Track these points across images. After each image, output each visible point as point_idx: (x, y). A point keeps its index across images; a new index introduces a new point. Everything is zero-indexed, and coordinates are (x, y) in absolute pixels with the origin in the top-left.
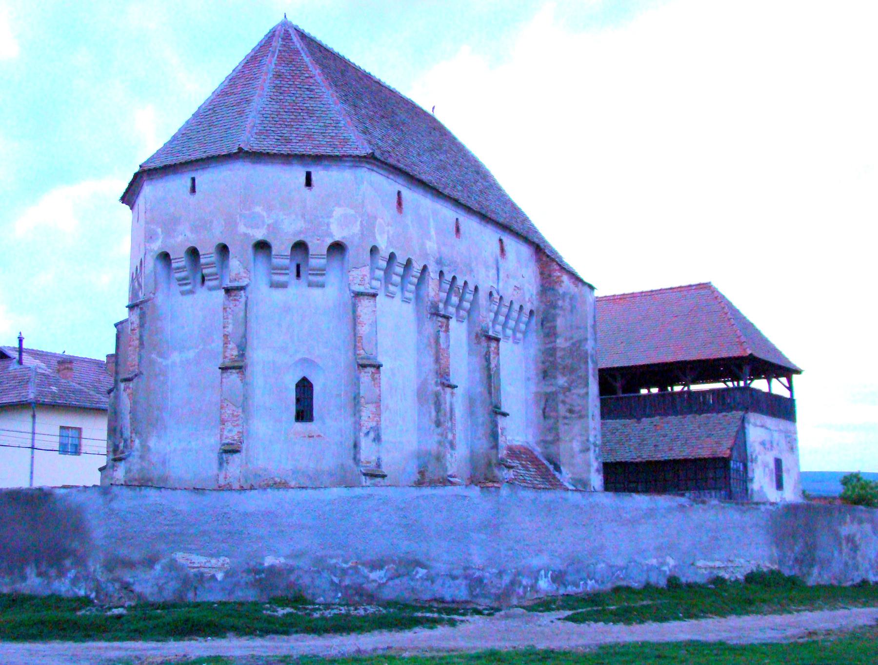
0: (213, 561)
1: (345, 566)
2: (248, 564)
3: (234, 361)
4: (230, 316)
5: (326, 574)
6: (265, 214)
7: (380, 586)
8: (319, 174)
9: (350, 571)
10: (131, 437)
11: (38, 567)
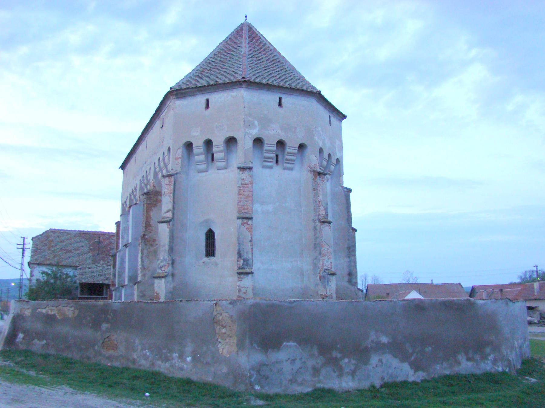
11: (466, 354)
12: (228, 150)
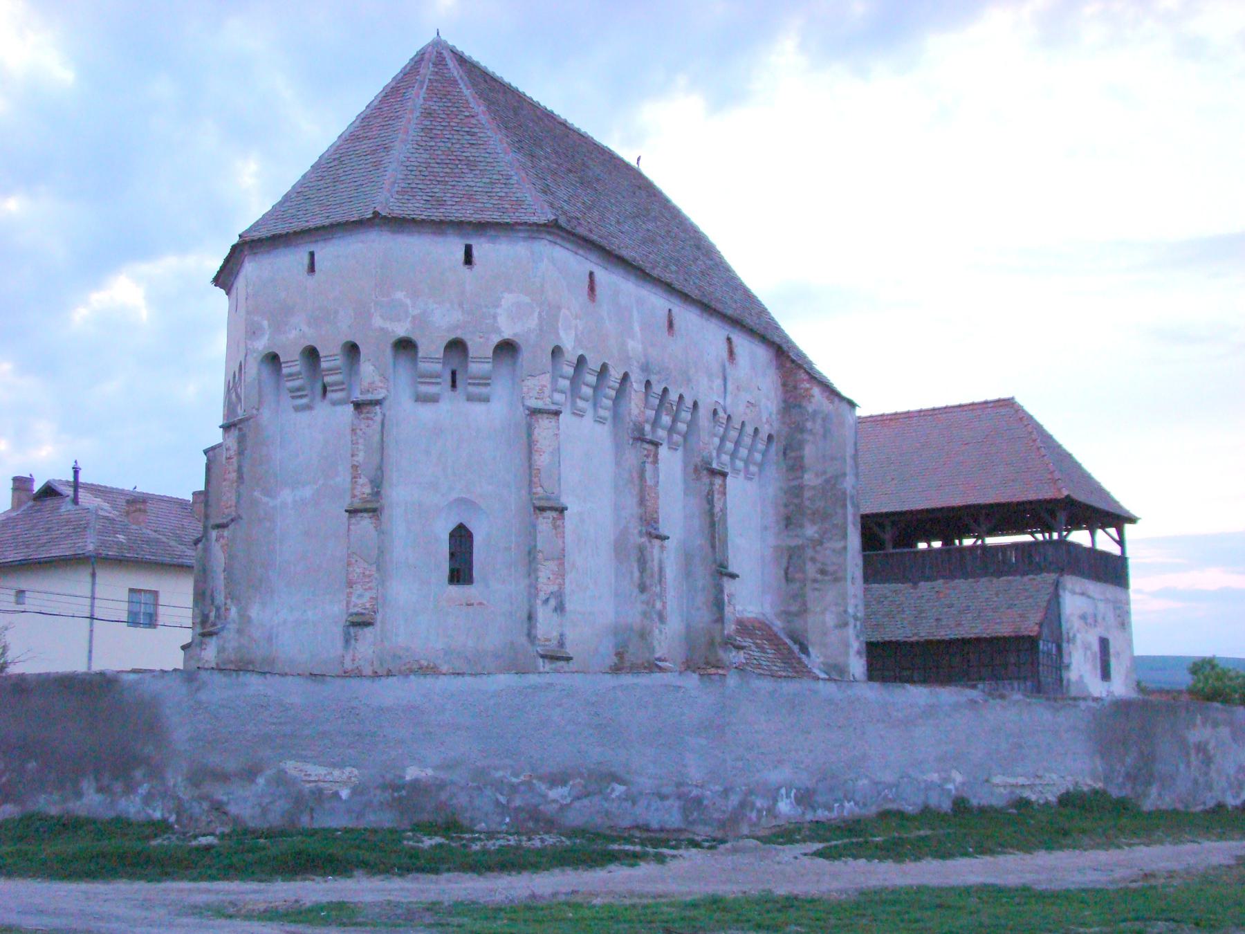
0: (336, 773)
1: (514, 780)
2: (383, 777)
3: (365, 501)
4: (361, 441)
5: (489, 792)
6: (408, 302)
7: (563, 808)
8: (482, 248)
9: (522, 788)
10: (226, 604)
11: (97, 780)
12: (314, 370)
